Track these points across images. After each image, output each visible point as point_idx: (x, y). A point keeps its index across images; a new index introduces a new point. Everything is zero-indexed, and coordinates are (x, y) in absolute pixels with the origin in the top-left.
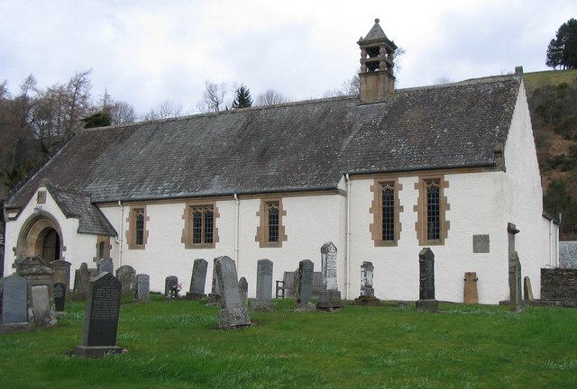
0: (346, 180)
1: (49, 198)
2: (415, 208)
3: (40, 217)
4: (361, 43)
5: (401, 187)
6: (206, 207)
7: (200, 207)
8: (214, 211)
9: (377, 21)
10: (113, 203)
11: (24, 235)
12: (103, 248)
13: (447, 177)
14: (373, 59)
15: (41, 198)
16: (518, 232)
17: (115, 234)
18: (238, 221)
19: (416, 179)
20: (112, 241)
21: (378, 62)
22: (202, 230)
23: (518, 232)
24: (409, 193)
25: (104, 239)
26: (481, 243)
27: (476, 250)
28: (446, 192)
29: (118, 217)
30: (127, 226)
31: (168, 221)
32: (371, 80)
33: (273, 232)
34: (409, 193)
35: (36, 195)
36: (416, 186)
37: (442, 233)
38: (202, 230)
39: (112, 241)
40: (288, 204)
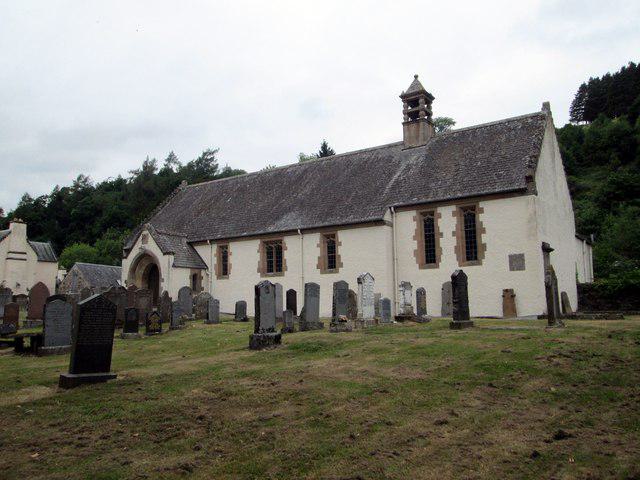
0: (392, 213)
1: (150, 239)
2: (454, 234)
3: (145, 256)
4: (404, 97)
5: (440, 216)
6: (276, 242)
7: (271, 242)
8: (283, 245)
9: (416, 77)
10: (204, 242)
11: (133, 270)
12: (195, 278)
13: (482, 204)
14: (414, 109)
15: (145, 238)
16: (552, 250)
17: (205, 267)
18: (302, 255)
19: (453, 208)
20: (203, 273)
21: (418, 112)
22: (274, 261)
23: (552, 250)
24: (448, 222)
25: (197, 271)
26: (517, 262)
27: (512, 269)
28: (482, 218)
29: (208, 254)
30: (215, 261)
31: (247, 257)
32: (413, 127)
33: (331, 262)
34: (448, 222)
35: (141, 238)
36: (454, 214)
37: (437, 258)
38: (274, 261)
39: (203, 273)
40: (343, 236)
